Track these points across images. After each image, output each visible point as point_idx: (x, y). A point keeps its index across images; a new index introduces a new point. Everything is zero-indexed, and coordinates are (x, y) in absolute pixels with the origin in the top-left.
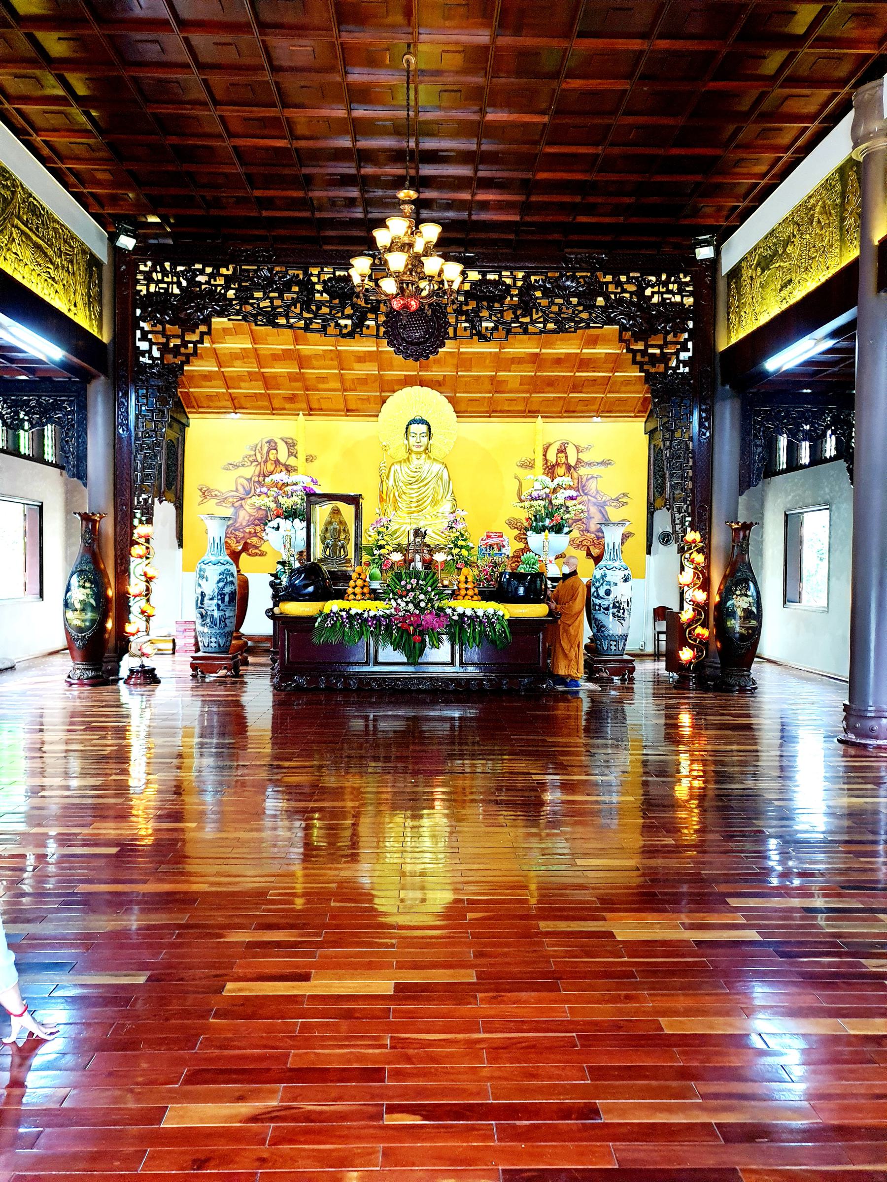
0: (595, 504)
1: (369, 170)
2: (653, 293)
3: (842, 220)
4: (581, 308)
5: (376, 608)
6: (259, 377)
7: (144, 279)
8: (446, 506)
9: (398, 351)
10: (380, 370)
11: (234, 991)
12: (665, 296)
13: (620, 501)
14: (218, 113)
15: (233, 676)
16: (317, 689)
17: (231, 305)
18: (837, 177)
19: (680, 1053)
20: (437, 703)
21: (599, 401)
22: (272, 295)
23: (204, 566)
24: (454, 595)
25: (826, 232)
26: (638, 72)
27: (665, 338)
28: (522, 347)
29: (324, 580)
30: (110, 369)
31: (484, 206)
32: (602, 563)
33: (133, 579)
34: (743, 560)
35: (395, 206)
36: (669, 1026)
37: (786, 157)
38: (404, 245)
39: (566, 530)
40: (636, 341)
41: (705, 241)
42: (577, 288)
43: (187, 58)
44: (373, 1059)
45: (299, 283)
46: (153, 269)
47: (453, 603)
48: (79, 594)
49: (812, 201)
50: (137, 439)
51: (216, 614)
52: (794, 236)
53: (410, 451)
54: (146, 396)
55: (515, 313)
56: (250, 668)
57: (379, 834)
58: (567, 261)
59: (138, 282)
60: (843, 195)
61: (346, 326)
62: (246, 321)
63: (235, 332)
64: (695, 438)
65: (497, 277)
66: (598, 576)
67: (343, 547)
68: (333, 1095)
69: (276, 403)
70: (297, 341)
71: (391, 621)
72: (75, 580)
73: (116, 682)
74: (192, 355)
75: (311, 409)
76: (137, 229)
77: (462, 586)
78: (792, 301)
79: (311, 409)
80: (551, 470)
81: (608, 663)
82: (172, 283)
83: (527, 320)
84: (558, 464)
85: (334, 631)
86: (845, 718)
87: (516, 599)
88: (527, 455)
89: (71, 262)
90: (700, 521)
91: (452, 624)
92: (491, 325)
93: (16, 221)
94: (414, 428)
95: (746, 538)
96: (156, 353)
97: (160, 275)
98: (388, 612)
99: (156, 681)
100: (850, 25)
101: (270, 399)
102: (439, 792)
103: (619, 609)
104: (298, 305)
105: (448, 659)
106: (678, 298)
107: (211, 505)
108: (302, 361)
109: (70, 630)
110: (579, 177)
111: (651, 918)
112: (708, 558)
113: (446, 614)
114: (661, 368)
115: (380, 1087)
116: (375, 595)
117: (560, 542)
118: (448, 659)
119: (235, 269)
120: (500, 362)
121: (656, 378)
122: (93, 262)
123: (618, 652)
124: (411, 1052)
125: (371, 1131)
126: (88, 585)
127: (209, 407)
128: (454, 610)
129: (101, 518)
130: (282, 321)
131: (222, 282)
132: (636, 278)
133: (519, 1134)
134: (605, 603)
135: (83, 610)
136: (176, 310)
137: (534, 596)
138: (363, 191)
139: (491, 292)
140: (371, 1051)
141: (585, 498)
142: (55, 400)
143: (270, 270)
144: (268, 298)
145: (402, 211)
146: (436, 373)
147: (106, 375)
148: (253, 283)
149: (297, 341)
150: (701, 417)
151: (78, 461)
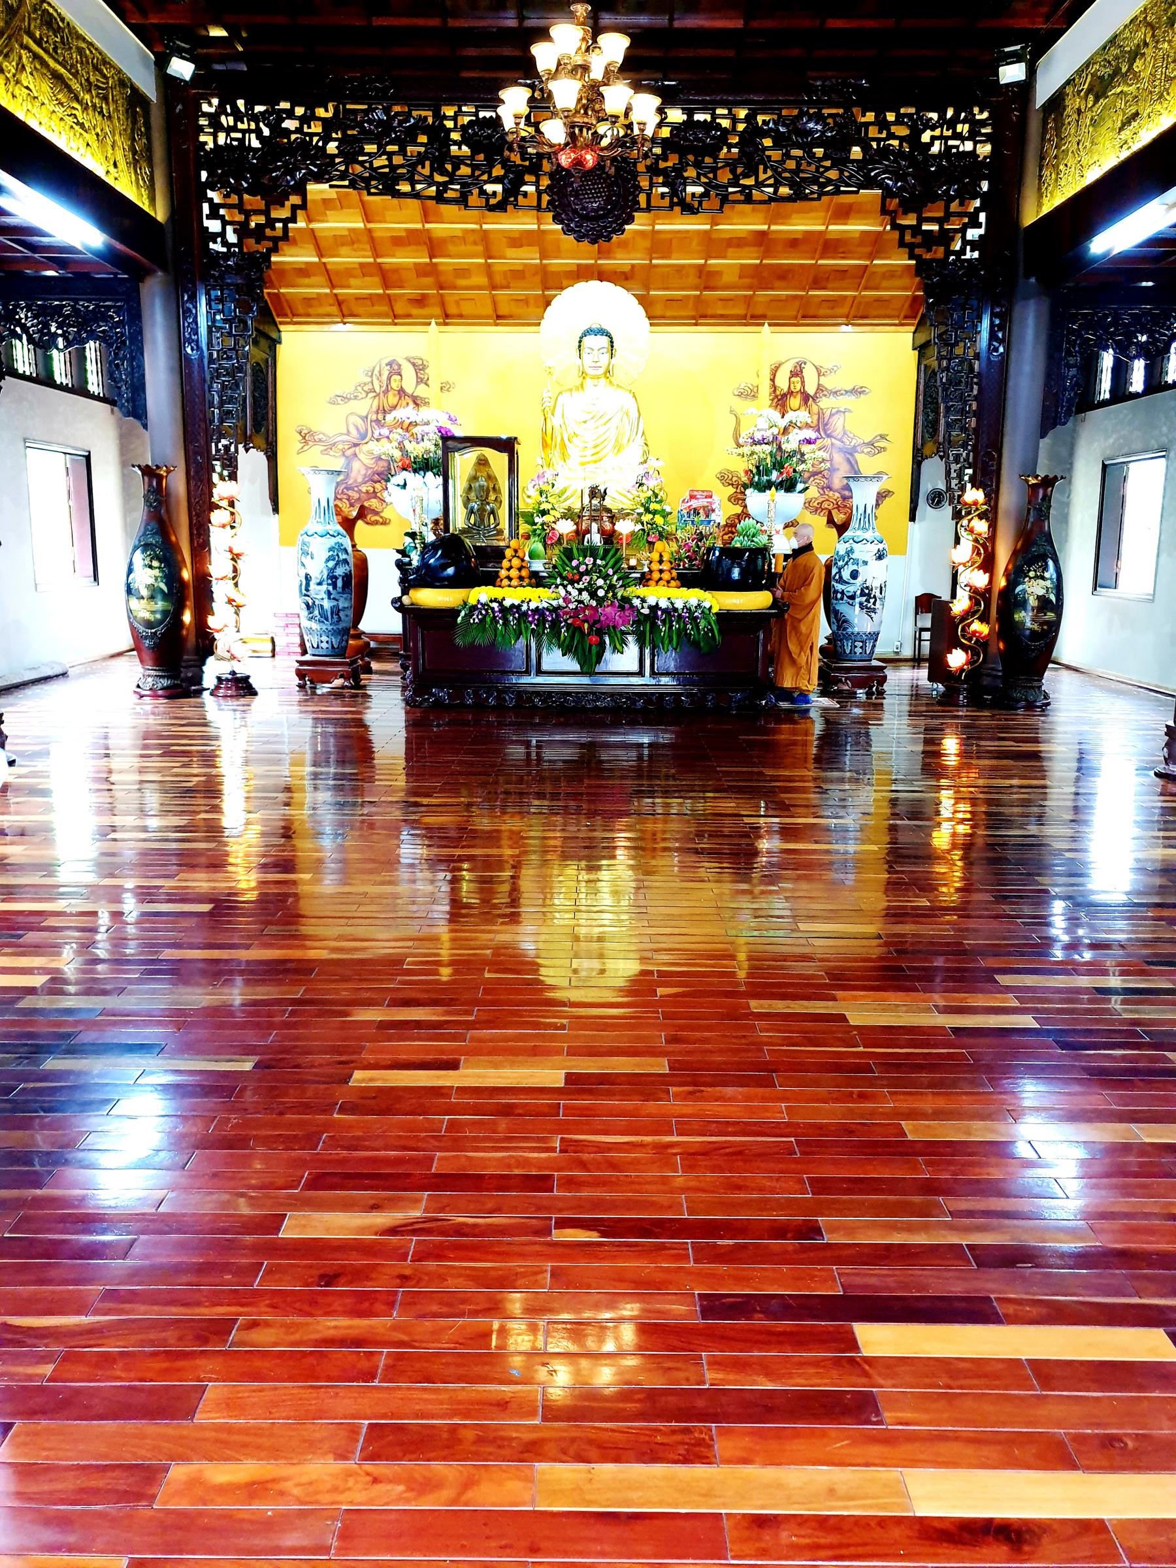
0: (840, 450)
2: (933, 138)
5: (539, 598)
7: (210, 126)
9: (567, 230)
11: (363, 1080)
12: (951, 143)
13: (875, 446)
15: (351, 688)
16: (463, 705)
21: (849, 301)
22: (390, 148)
23: (307, 539)
24: (644, 580)
27: (947, 207)
28: (743, 223)
29: (468, 558)
32: (848, 534)
34: (1042, 527)
36: (913, 1131)
38: (576, 68)
39: (800, 486)
42: (823, 132)
45: (426, 130)
46: (221, 110)
47: (641, 591)
48: (147, 576)
52: (1146, 45)
55: (733, 171)
57: (545, 889)
59: (201, 129)
61: (495, 193)
63: (340, 204)
64: (984, 354)
65: (708, 118)
66: (842, 552)
67: (493, 512)
70: (426, 218)
71: (558, 616)
73: (198, 693)
77: (655, 566)
78: (1136, 146)
80: (781, 401)
81: (851, 671)
82: (249, 131)
83: (750, 182)
84: (790, 393)
86: (1167, 745)
88: (752, 381)
89: (105, 99)
91: (640, 620)
92: (699, 190)
93: (26, 40)
95: (1047, 499)
96: (232, 238)
97: (231, 120)
98: (555, 603)
103: (869, 598)
104: (427, 163)
106: (968, 146)
107: (314, 454)
108: (434, 246)
109: (136, 625)
111: (894, 998)
113: (632, 607)
114: (940, 252)
116: (537, 580)
117: (791, 503)
118: (635, 668)
119: (336, 109)
122: (136, 99)
123: (865, 657)
124: (585, 1156)
125: (537, 1248)
126: (155, 564)
127: (309, 315)
128: (643, 600)
129: (168, 472)
130: (405, 187)
131: (319, 130)
132: (910, 116)
134: (850, 589)
135: (152, 597)
139: (697, 139)
140: (536, 1155)
142: (97, 306)
143: (387, 111)
146: (620, 261)
147: (164, 269)
148: (363, 131)
149: (426, 218)
150: (992, 323)
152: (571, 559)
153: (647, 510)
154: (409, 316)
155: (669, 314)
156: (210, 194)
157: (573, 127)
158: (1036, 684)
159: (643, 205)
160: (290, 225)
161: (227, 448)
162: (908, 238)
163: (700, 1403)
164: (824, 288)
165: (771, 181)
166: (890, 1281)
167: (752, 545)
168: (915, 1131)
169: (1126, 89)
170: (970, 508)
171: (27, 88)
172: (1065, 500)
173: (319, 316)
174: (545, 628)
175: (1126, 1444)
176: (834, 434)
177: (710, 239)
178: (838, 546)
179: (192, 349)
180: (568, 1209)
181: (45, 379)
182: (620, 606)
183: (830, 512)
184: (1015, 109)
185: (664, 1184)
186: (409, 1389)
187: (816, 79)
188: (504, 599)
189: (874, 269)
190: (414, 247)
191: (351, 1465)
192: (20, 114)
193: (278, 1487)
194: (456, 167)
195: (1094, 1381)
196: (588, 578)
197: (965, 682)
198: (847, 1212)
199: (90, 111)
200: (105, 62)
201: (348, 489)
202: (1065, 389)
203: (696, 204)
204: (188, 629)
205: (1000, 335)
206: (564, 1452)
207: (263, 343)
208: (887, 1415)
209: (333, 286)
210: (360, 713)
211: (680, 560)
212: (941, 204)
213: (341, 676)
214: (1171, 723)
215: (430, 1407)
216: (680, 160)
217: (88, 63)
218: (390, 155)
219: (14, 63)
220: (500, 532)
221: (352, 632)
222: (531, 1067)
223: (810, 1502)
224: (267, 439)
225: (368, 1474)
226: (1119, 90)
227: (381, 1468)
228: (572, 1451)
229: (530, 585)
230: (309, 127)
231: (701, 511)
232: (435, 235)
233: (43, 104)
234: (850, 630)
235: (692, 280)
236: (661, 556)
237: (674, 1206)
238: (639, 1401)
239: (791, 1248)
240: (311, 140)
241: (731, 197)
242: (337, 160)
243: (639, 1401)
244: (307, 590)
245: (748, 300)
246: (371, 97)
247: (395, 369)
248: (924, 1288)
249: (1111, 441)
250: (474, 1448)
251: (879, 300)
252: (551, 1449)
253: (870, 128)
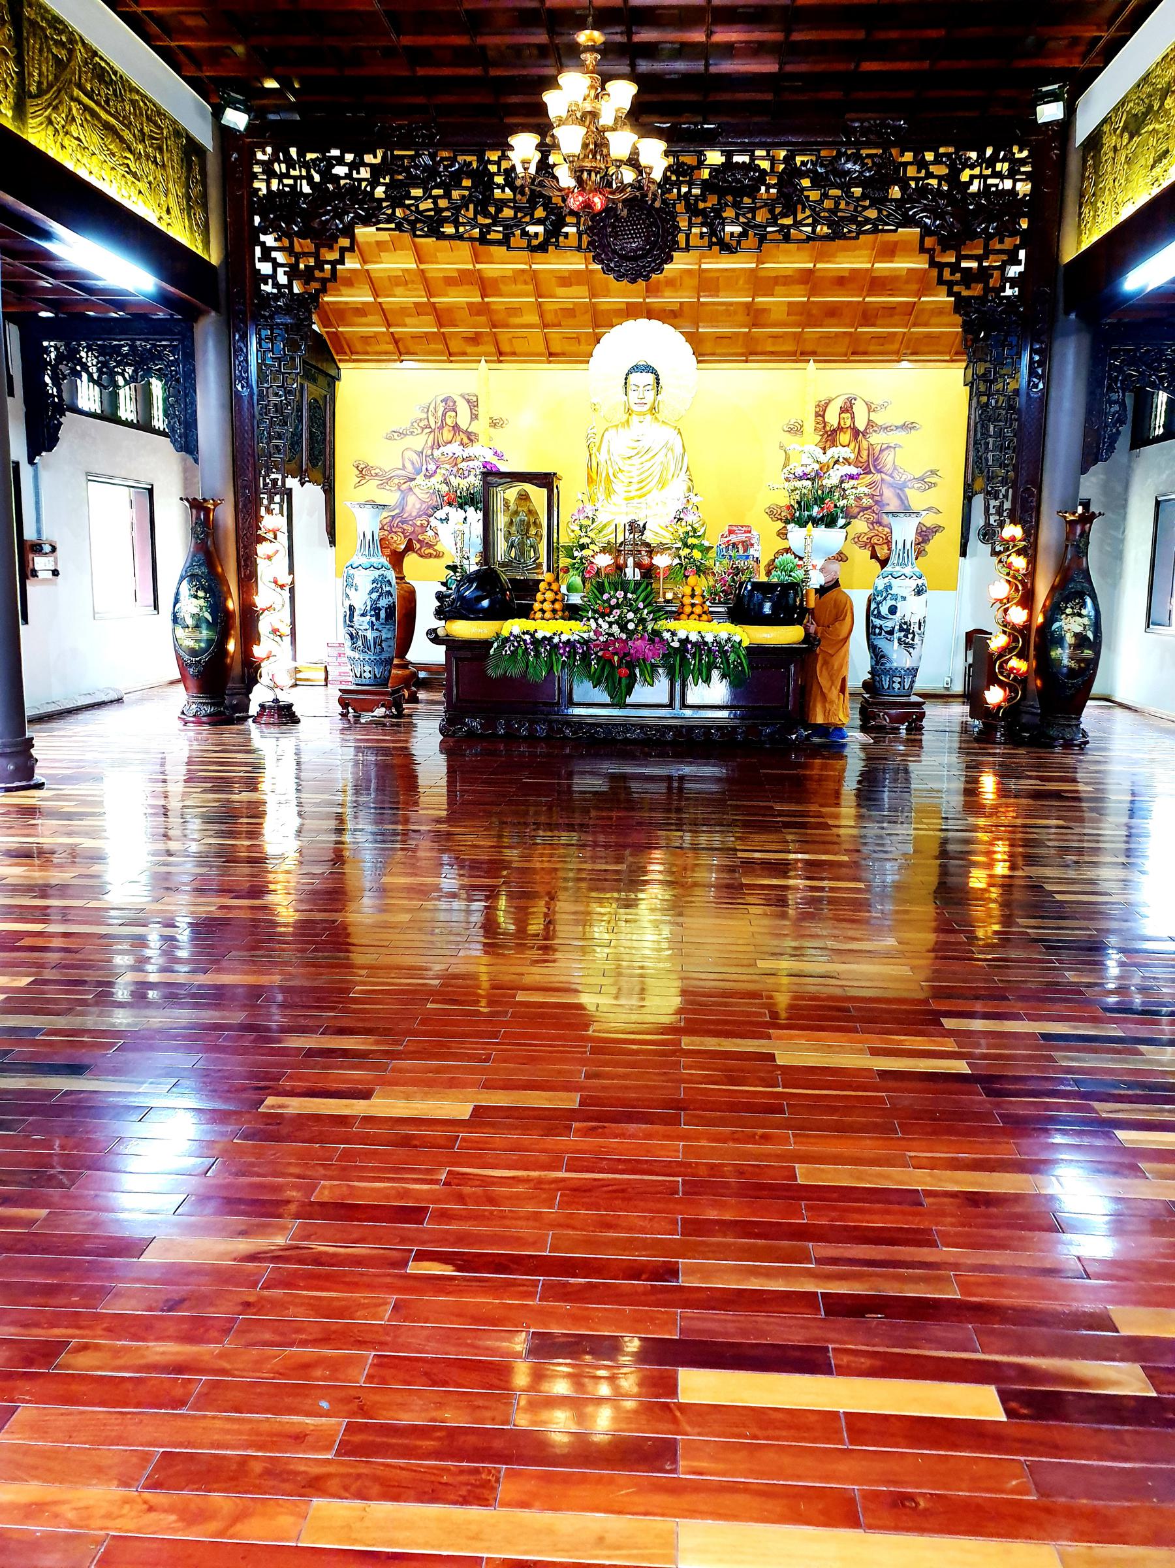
0: (891, 485)
2: (972, 177)
5: (570, 630)
6: (429, 309)
7: (263, 173)
9: (607, 270)
10: (593, 295)
11: (273, 1107)
12: (990, 181)
13: (926, 482)
15: (393, 716)
16: (494, 735)
17: (380, 208)
19: (808, 1208)
22: (436, 192)
23: (352, 571)
24: (677, 615)
27: (986, 246)
28: (788, 261)
30: (223, 302)
31: (729, 50)
32: (888, 569)
35: (570, 55)
36: (804, 1175)
39: (841, 522)
40: (943, 251)
42: (861, 173)
45: (471, 174)
46: (274, 158)
47: (672, 625)
48: (192, 606)
50: (261, 396)
51: (370, 635)
53: (629, 411)
54: (271, 339)
55: (772, 211)
56: (419, 706)
59: (255, 176)
61: (536, 234)
62: (401, 231)
63: (395, 246)
64: (1023, 391)
65: (746, 159)
69: (455, 346)
70: (477, 259)
71: (589, 648)
73: (244, 719)
74: (329, 280)
75: (501, 354)
77: (687, 600)
80: (830, 436)
81: (891, 710)
83: (788, 221)
84: (840, 428)
85: (515, 661)
89: (160, 149)
90: (1024, 510)
92: (738, 229)
94: (635, 378)
95: (1085, 535)
96: (282, 279)
97: (283, 166)
98: (585, 636)
102: (656, 871)
103: (908, 633)
104: (471, 206)
105: (665, 700)
106: (1008, 184)
107: (371, 491)
108: (485, 286)
112: (1032, 561)
113: (662, 640)
114: (977, 290)
115: (417, 1230)
116: (573, 612)
117: (831, 539)
118: (665, 700)
119: (384, 157)
120: (760, 283)
121: (970, 305)
122: (192, 149)
123: (903, 692)
124: (467, 1190)
125: (388, 1280)
126: (201, 594)
127: (367, 353)
128: (674, 634)
129: (216, 505)
130: (449, 230)
131: (368, 176)
132: (948, 155)
133: (569, 1293)
134: (888, 625)
135: (197, 626)
139: (739, 181)
140: (417, 1187)
141: (877, 477)
142: (154, 346)
143: (432, 156)
144: (430, 196)
146: (669, 299)
147: (217, 310)
149: (477, 259)
150: (1031, 358)
152: (602, 593)
154: (464, 354)
156: (262, 238)
157: (582, 171)
159: (683, 245)
160: (339, 267)
161: (275, 481)
163: (498, 1444)
164: (873, 325)
165: (810, 221)
166: (731, 1327)
169: (1157, 126)
170: (1008, 544)
171: (78, 139)
172: (1120, 536)
174: (575, 660)
175: (917, 1504)
176: (884, 470)
177: (756, 277)
178: (877, 581)
179: (243, 387)
181: (110, 415)
182: (650, 640)
183: (873, 548)
184: (1055, 148)
185: (536, 1220)
186: (214, 1418)
188: (536, 631)
189: (922, 307)
190: (466, 287)
191: (132, 1492)
192: (70, 165)
193: (56, 1509)
194: (499, 210)
195: (906, 1437)
196: (618, 611)
197: (1002, 719)
198: (710, 1255)
200: (160, 113)
201: (403, 522)
202: (1106, 426)
203: (734, 244)
204: (232, 658)
205: (1040, 371)
206: (346, 1488)
207: (321, 380)
208: (682, 1463)
209: (389, 326)
210: (407, 741)
211: (716, 594)
212: (980, 242)
215: (229, 1437)
217: (141, 114)
218: (435, 199)
219: (63, 115)
220: (540, 565)
221: (396, 662)
223: (577, 1550)
224: (324, 474)
225: (145, 1502)
226: (1151, 127)
227: (159, 1497)
228: (354, 1488)
229: (563, 618)
230: (358, 173)
231: (740, 546)
233: (94, 154)
234: (888, 665)
235: (741, 317)
236: (693, 590)
237: (537, 1243)
238: (439, 1439)
239: (640, 1290)
240: (360, 185)
241: (769, 237)
242: (385, 204)
243: (439, 1439)
244: (351, 621)
245: (797, 337)
247: (450, 405)
248: (764, 1334)
249: (1164, 476)
250: (257, 1482)
251: (929, 336)
252: (333, 1484)
253: (909, 167)
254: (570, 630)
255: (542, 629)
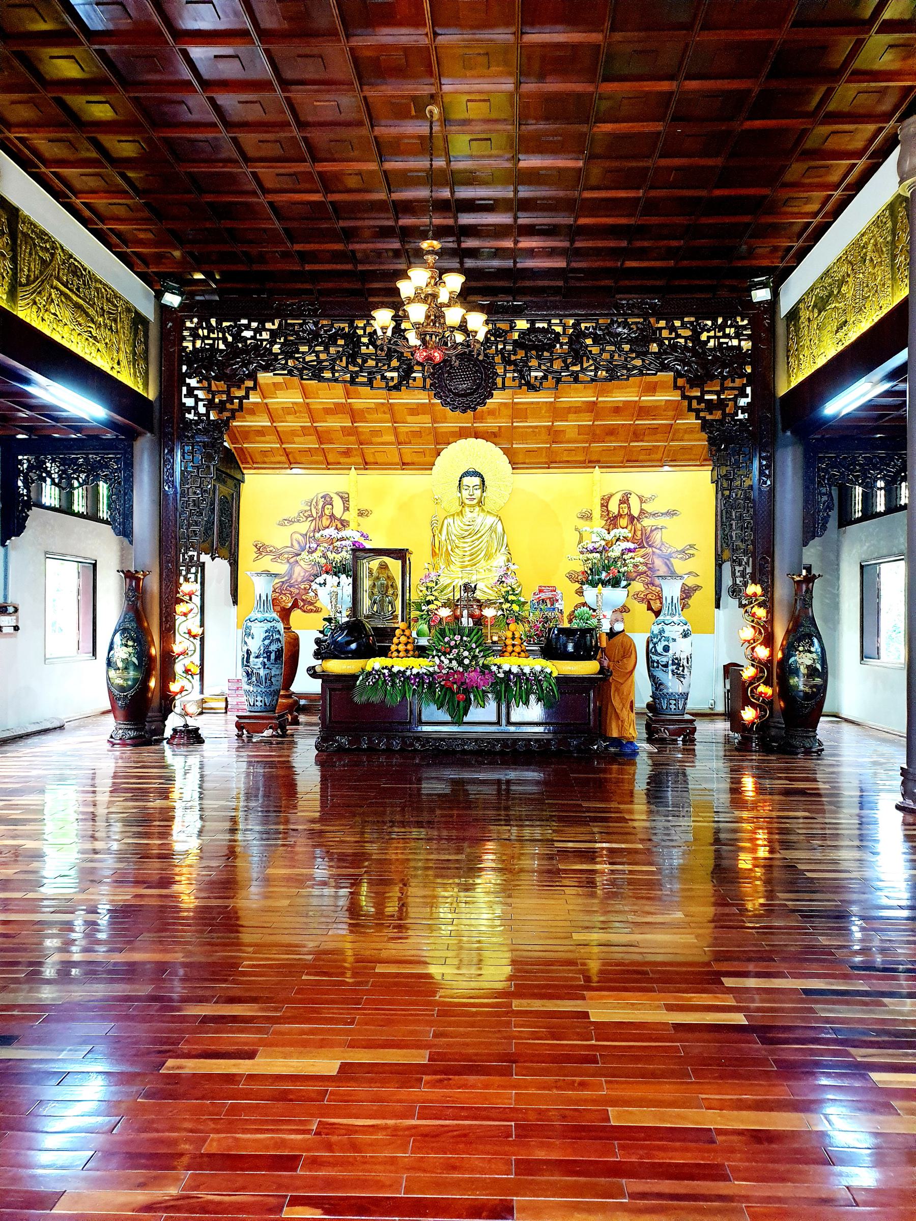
0: (659, 556)
1: (405, 221)
2: (709, 338)
3: (894, 257)
4: (634, 355)
5: (420, 665)
6: (312, 431)
8: (500, 560)
9: (445, 404)
11: (173, 1068)
12: (722, 340)
13: (687, 553)
14: (249, 170)
17: (276, 360)
18: (887, 214)
20: (481, 763)
23: (249, 624)
24: (502, 653)
25: (878, 271)
26: (670, 112)
27: (722, 385)
29: (367, 636)
32: (661, 618)
33: (178, 638)
34: (807, 614)
36: (617, 1117)
37: (837, 194)
38: (427, 296)
39: (624, 583)
40: (691, 387)
41: (760, 283)
43: (213, 118)
44: (292, 1145)
45: (344, 336)
46: (199, 326)
47: (498, 660)
48: (122, 653)
49: (865, 239)
51: (262, 672)
52: (848, 276)
53: (463, 504)
54: (192, 452)
55: (565, 361)
56: (300, 727)
57: (431, 902)
58: (618, 306)
59: (184, 338)
60: (894, 232)
61: (392, 378)
64: (756, 487)
65: (546, 325)
66: (656, 632)
68: (238, 1185)
70: (348, 395)
71: (434, 679)
72: (118, 637)
75: (366, 463)
76: (183, 285)
77: (509, 642)
78: (847, 343)
79: (366, 463)
80: (612, 521)
81: (669, 725)
82: (218, 339)
83: (577, 368)
84: (620, 515)
86: (903, 783)
87: (566, 656)
88: (585, 508)
89: (115, 320)
91: (497, 682)
93: (55, 282)
94: (467, 481)
95: (809, 591)
96: (202, 410)
97: (206, 332)
98: (431, 669)
99: (200, 741)
100: (888, 57)
101: (325, 454)
102: (489, 859)
103: (679, 667)
104: (344, 359)
105: (494, 719)
106: (735, 342)
107: (267, 563)
108: (354, 415)
109: (113, 689)
110: (623, 221)
112: (771, 612)
113: (491, 671)
114: (718, 415)
115: (291, 1176)
116: (421, 652)
117: (617, 596)
118: (494, 719)
122: (139, 320)
124: (334, 1138)
126: (130, 643)
127: (265, 463)
128: (499, 667)
129: (145, 576)
131: (268, 337)
132: (691, 323)
134: (664, 660)
135: (126, 668)
136: (222, 365)
137: (584, 652)
138: (403, 242)
139: (540, 341)
140: (293, 1137)
141: (649, 550)
142: (103, 458)
143: (316, 324)
144: (314, 352)
145: (425, 262)
146: (491, 424)
147: (152, 432)
148: (298, 337)
150: (760, 464)
151: (124, 519)
152: (444, 636)
153: (507, 601)
155: (527, 461)
158: (812, 734)
162: (694, 404)
167: (587, 626)
168: (618, 1117)
171: (55, 314)
172: (836, 592)
173: (271, 463)
180: (304, 1188)
181: (66, 509)
182: (481, 672)
183: (649, 603)
187: (622, 300)
188: (393, 666)
190: (341, 415)
194: (365, 361)
199: (102, 329)
200: (116, 296)
205: (767, 472)
212: (718, 381)
213: (271, 728)
214: (905, 766)
216: (526, 354)
221: (282, 693)
222: (314, 1057)
224: (230, 551)
226: (833, 306)
230: (261, 335)
232: (355, 407)
235: (544, 436)
236: (513, 634)
240: (262, 344)
242: (280, 357)
244: (248, 661)
246: (305, 316)
249: (865, 548)
251: (683, 448)
254: (420, 665)
255: (397, 664)
